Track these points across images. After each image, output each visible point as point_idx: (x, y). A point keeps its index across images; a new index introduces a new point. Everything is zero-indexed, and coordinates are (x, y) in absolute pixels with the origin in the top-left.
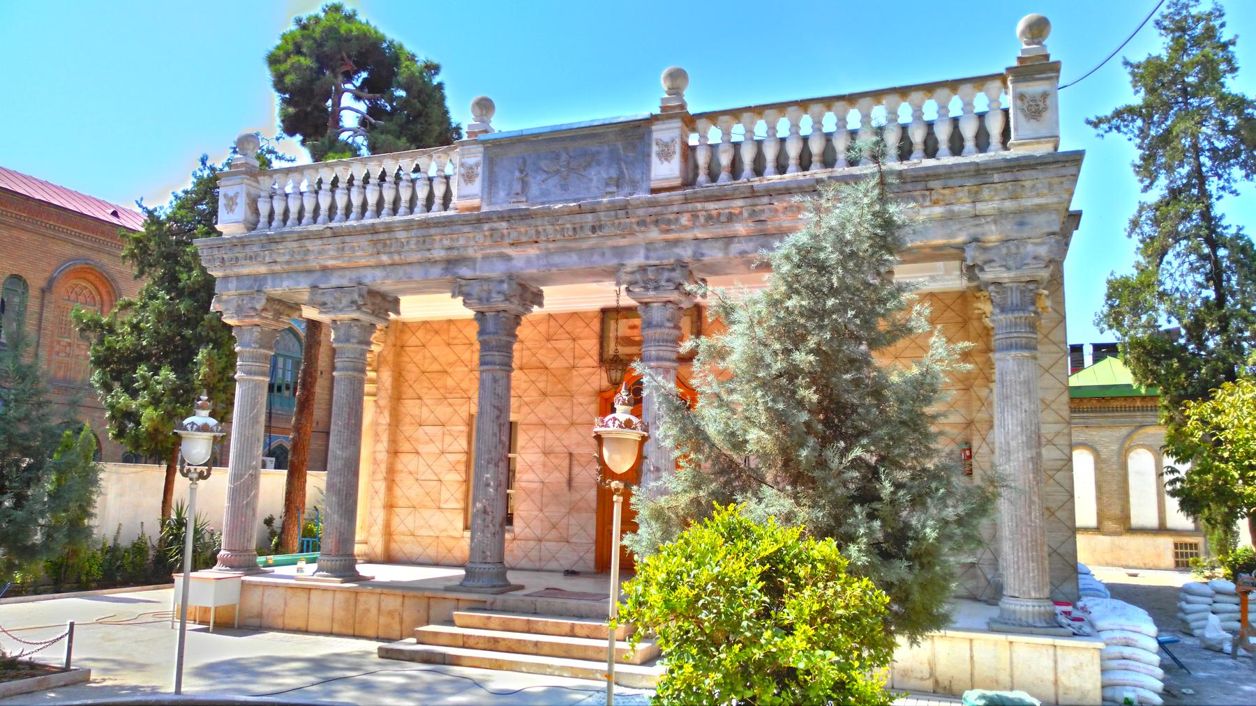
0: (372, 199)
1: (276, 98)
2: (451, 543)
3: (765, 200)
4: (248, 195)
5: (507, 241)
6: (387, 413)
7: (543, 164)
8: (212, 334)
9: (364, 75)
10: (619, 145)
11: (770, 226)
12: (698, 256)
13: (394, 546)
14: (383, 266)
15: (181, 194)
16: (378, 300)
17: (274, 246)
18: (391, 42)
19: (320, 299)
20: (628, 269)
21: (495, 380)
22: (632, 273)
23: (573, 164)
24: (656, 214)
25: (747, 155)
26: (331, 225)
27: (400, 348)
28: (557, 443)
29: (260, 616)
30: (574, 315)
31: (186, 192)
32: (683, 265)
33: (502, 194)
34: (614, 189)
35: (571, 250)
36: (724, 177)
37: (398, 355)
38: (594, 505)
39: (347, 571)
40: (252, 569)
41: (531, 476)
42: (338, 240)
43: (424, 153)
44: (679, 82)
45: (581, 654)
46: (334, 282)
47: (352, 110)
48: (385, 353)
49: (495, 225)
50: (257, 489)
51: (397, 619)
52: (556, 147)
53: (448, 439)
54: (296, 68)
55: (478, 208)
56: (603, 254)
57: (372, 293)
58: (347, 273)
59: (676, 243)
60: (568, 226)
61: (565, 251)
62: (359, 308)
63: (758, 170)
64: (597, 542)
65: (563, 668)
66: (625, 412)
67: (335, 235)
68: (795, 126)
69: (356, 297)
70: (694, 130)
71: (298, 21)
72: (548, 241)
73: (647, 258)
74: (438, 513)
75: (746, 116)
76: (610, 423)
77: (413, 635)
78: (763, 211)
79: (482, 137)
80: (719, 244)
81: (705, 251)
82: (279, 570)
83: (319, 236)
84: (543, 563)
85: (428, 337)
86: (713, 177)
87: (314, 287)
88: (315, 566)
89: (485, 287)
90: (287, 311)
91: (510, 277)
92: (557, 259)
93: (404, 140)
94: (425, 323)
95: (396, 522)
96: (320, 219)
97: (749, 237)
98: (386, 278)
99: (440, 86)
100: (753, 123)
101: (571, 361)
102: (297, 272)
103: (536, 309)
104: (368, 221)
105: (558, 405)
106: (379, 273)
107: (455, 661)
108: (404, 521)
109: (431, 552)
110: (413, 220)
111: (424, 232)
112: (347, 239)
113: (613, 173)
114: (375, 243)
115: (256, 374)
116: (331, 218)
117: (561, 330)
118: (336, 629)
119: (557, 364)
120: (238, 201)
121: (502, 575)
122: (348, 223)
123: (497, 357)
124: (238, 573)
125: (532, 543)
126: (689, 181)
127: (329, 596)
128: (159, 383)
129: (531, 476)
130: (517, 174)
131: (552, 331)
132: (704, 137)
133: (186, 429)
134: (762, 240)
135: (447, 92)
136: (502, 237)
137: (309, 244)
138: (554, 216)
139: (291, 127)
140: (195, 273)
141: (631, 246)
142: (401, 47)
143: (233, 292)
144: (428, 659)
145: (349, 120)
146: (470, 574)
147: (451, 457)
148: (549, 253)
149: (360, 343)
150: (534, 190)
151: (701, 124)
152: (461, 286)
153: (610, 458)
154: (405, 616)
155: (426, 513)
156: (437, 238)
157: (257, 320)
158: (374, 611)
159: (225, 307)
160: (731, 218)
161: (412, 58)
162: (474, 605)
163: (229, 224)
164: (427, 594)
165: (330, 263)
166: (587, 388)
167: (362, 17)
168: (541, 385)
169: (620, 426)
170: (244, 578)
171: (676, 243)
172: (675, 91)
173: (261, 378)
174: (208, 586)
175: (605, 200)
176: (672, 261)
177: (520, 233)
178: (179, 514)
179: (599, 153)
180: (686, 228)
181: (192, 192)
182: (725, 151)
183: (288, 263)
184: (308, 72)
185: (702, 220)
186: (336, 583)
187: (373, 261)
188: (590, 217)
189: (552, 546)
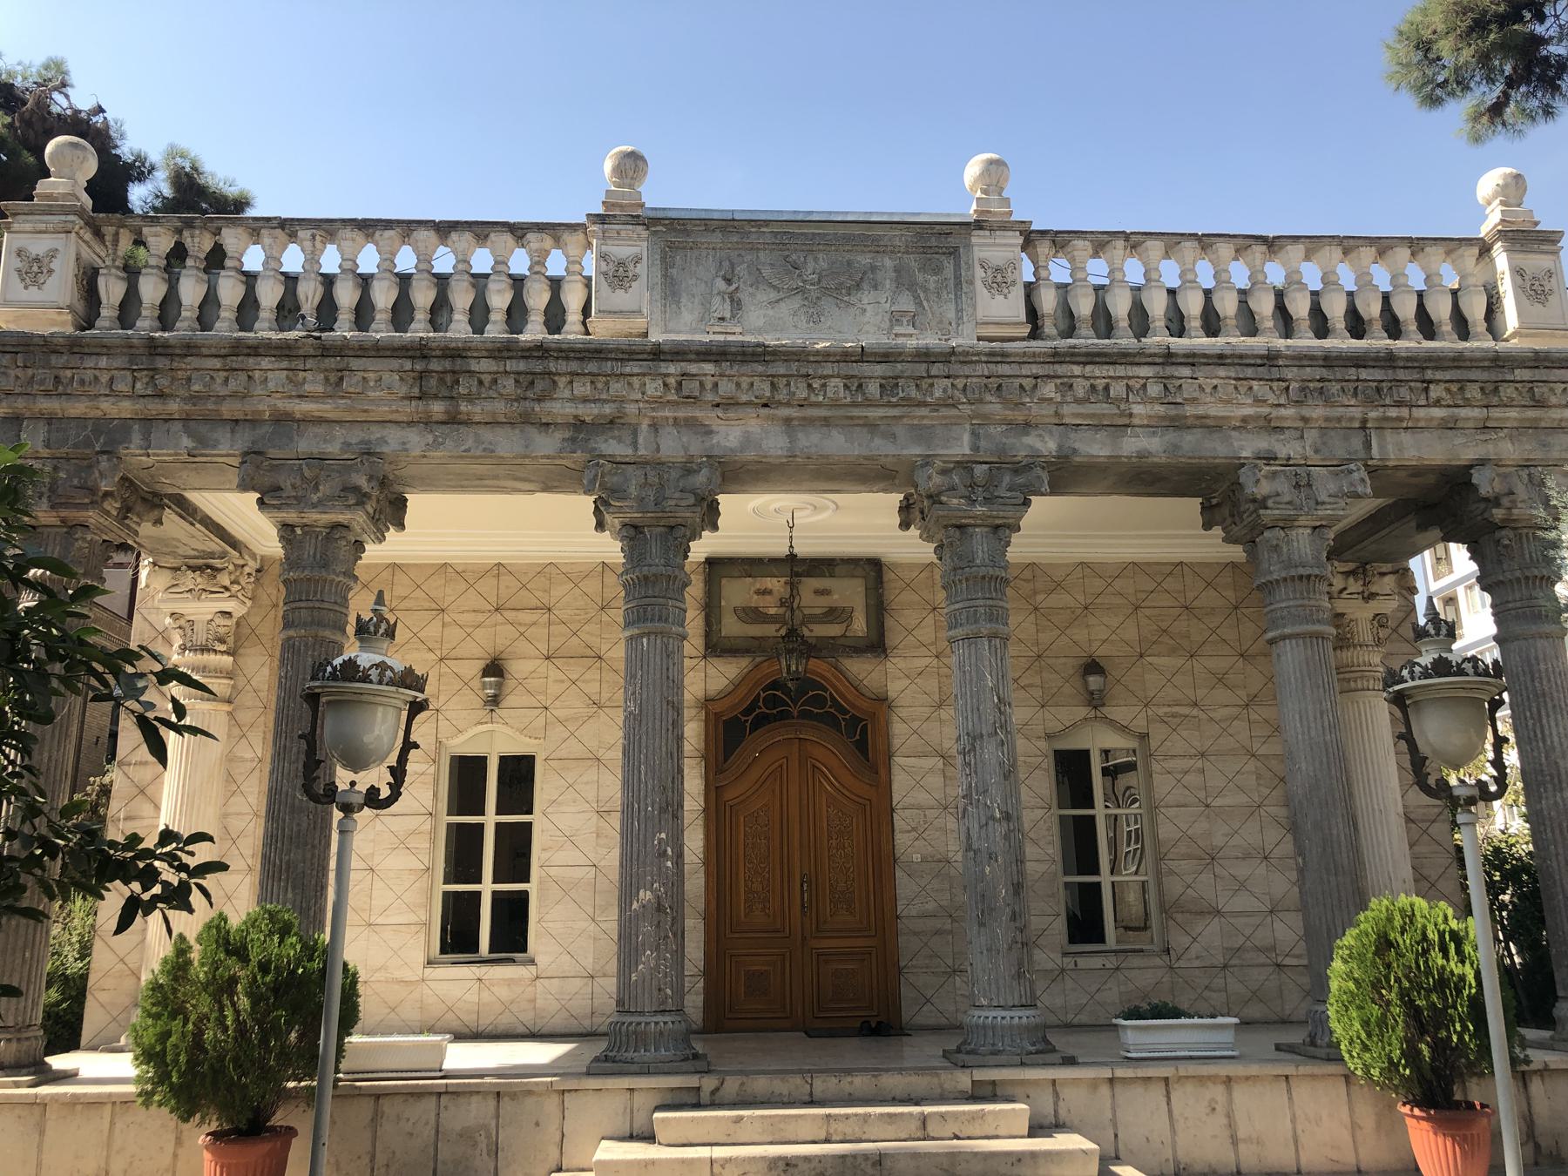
41: (572, 856)
46: (306, 444)
49: (693, 368)
58: (339, 432)
73: (975, 448)
98: (436, 444)
112: (355, 364)
129: (572, 856)
130: (720, 284)
133: (366, 679)
156: (562, 381)
162: (669, 1099)
168: (592, 688)
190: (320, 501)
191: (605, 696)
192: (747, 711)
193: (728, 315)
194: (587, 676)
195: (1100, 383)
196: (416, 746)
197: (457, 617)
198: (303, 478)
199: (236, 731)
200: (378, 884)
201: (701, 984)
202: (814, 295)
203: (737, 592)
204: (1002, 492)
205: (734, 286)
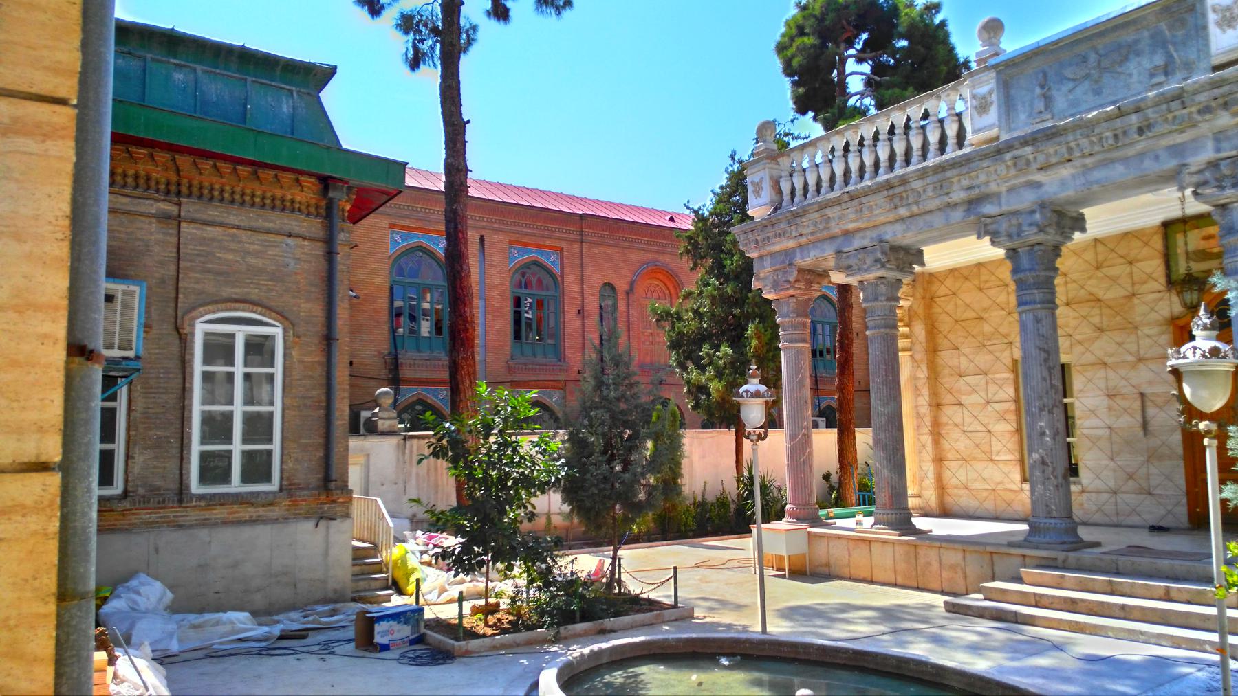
2: (1009, 496)
4: (771, 178)
5: (1034, 166)
6: (924, 367)
7: (1068, 73)
9: (864, 36)
10: (1163, 26)
13: (948, 500)
14: (902, 220)
16: (901, 255)
19: (845, 262)
20: (1193, 169)
21: (1038, 320)
22: (1200, 172)
24: (1223, 96)
27: (929, 301)
28: (1124, 383)
29: (828, 565)
30: (1126, 235)
31: (722, 188)
33: (1023, 117)
34: (1162, 78)
35: (1113, 161)
38: (1180, 450)
40: (816, 521)
42: (855, 202)
43: (932, 95)
46: (857, 243)
48: (915, 307)
49: (1017, 153)
51: (960, 574)
52: (1081, 49)
55: (997, 138)
56: (1157, 158)
57: (895, 249)
58: (868, 233)
60: (1108, 134)
62: (883, 266)
64: (1188, 493)
67: (852, 198)
69: (879, 255)
72: (1083, 156)
73: (1218, 150)
74: (991, 464)
76: (1189, 354)
77: (979, 591)
79: (993, 61)
82: (839, 523)
83: (837, 202)
84: (1121, 518)
85: (958, 285)
88: (871, 520)
89: (1014, 221)
91: (1042, 206)
92: (1097, 175)
93: (911, 89)
94: (952, 271)
95: (947, 475)
98: (908, 229)
99: (943, 24)
101: (1130, 289)
102: (822, 240)
103: (1077, 235)
105: (1119, 340)
106: (899, 227)
108: (956, 475)
109: (989, 505)
111: (940, 176)
112: (864, 200)
113: (1159, 60)
115: (797, 341)
116: (846, 183)
118: (900, 581)
119: (1112, 294)
121: (1073, 530)
123: (1037, 295)
125: (1105, 496)
127: (889, 548)
129: (1094, 422)
130: (1038, 91)
131: (1101, 258)
136: (1028, 163)
138: (1091, 125)
139: (802, 107)
141: (1194, 140)
145: (855, 84)
146: (1034, 529)
147: (997, 406)
148: (1086, 170)
149: (888, 300)
150: (1060, 102)
152: (986, 225)
153: (1193, 394)
154: (968, 570)
155: (979, 466)
156: (955, 180)
157: (791, 292)
158: (935, 565)
159: (764, 285)
162: (1044, 562)
163: (758, 209)
164: (989, 549)
165: (851, 226)
166: (1154, 316)
168: (1096, 320)
169: (1204, 355)
170: (810, 530)
174: (780, 536)
175: (1151, 94)
177: (1048, 156)
179: (1136, 42)
181: (727, 186)
183: (812, 233)
186: (894, 536)
187: (891, 217)
188: (1134, 118)
189: (1131, 499)
193: (1043, 109)
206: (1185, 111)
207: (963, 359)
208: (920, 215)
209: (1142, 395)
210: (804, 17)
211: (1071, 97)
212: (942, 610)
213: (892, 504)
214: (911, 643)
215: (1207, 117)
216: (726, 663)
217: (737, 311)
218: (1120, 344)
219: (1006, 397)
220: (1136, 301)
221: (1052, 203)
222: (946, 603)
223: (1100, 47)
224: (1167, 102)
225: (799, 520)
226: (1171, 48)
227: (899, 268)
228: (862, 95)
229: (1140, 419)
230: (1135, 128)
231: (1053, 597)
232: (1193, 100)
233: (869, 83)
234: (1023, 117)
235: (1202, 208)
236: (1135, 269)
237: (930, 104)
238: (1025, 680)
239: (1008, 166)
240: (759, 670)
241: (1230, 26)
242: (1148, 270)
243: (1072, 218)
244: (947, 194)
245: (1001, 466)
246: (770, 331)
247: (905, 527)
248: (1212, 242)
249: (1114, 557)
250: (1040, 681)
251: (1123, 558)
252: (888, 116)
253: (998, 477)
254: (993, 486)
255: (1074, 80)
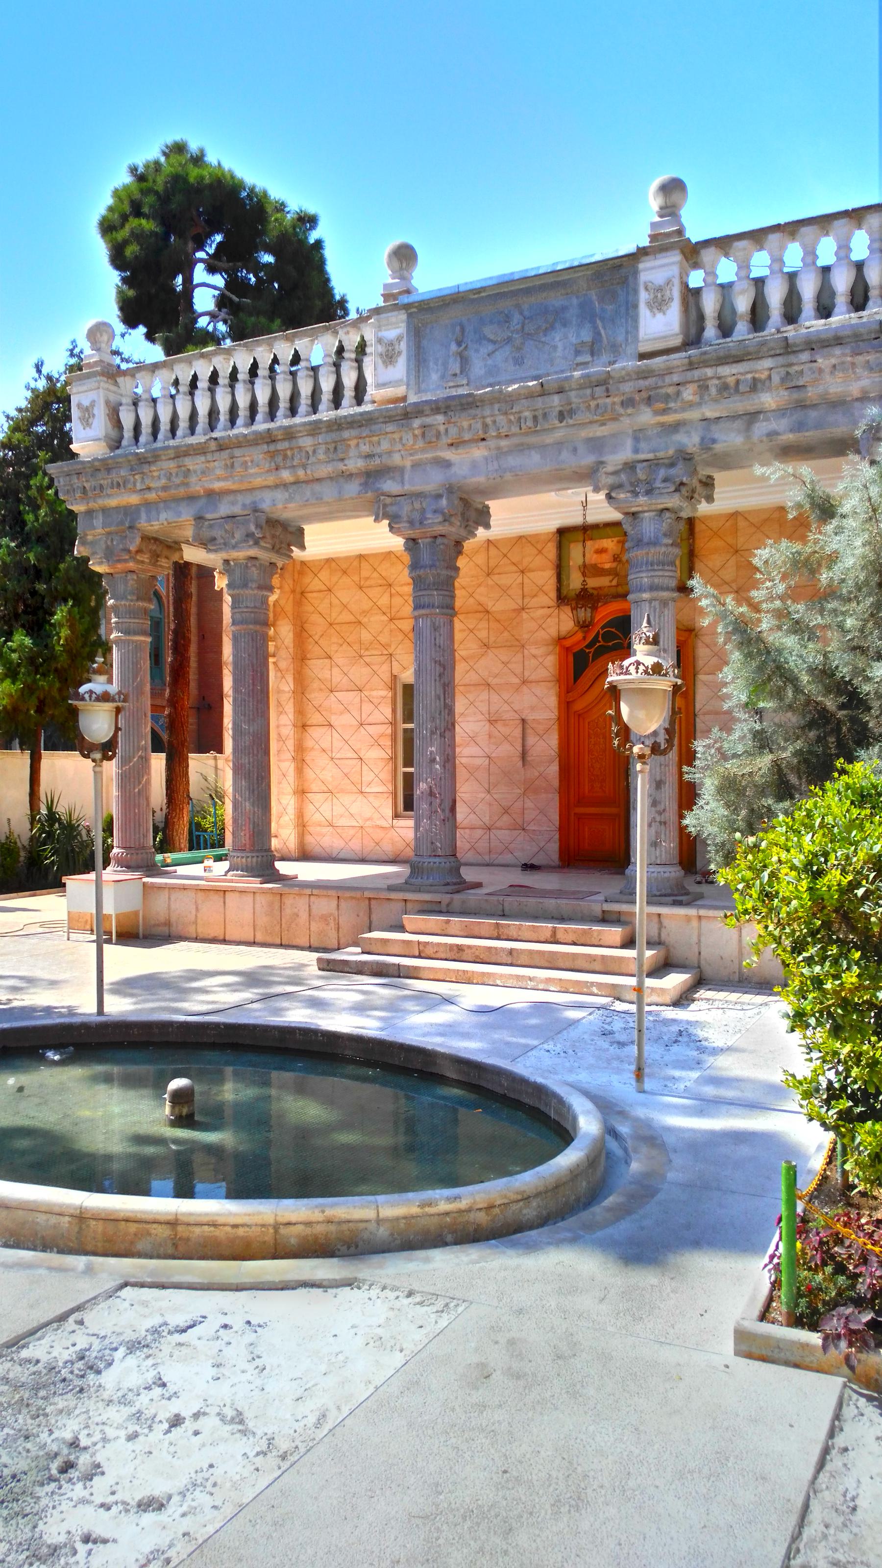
0: (263, 396)
1: (114, 277)
2: (378, 835)
3: (805, 356)
4: (107, 402)
5: (445, 440)
6: (290, 679)
7: (488, 331)
8: (69, 588)
9: (218, 238)
10: (593, 295)
11: (812, 393)
12: (707, 444)
13: (309, 839)
14: (285, 486)
15: (14, 413)
16: (279, 531)
17: (146, 468)
18: (252, 190)
19: (207, 533)
20: (610, 468)
21: (435, 628)
22: (616, 473)
23: (530, 328)
24: (648, 389)
25: (775, 296)
26: (215, 434)
27: (300, 595)
28: (506, 707)
29: (168, 923)
30: (520, 539)
31: (20, 410)
32: (686, 457)
33: (435, 377)
34: (587, 358)
35: (530, 447)
36: (742, 329)
37: (298, 604)
38: (556, 783)
39: (265, 869)
40: (151, 869)
42: (225, 454)
43: (327, 329)
44: (675, 197)
45: (568, 965)
46: (224, 509)
47: (206, 292)
48: (282, 602)
49: (428, 420)
50: (149, 774)
51: (332, 925)
52: (506, 305)
53: (367, 708)
54: (137, 236)
55: (404, 399)
56: (575, 450)
57: (273, 523)
58: (240, 498)
59: (676, 427)
60: (527, 414)
61: (522, 448)
62: (256, 543)
63: (791, 315)
64: (561, 829)
65: (548, 980)
66: (649, 654)
67: (221, 448)
68: (844, 248)
69: (252, 528)
70: (696, 266)
71: (133, 170)
72: (499, 437)
73: (636, 451)
74: (360, 797)
75: (773, 238)
76: (632, 669)
77: (355, 944)
78: (802, 372)
79: (405, 299)
80: (738, 424)
81: (716, 436)
82: (181, 870)
83: (200, 450)
84: (494, 856)
85: (335, 579)
86: (725, 330)
87: (199, 518)
88: (225, 865)
89: (417, 505)
90: (166, 552)
91: (450, 490)
92: (512, 461)
93: (278, 322)
94: (329, 561)
95: (310, 809)
96: (199, 428)
97: (781, 412)
98: (290, 499)
99: (319, 244)
100: (783, 248)
101: (520, 602)
102: (177, 500)
103: (481, 532)
104: (261, 425)
105: (505, 658)
106: (280, 496)
107: (413, 974)
108: (321, 809)
109: (355, 845)
110: (320, 421)
111: (334, 436)
112: (237, 452)
113: (586, 335)
114: (272, 455)
115: (136, 633)
116: (212, 427)
117: (505, 560)
118: (259, 938)
119: (501, 606)
120: (96, 411)
121: (455, 870)
122: (235, 431)
123: (436, 597)
124: (137, 875)
125: (479, 832)
126: (693, 337)
127: (249, 898)
128: (14, 651)
130: (454, 347)
131: (492, 563)
132: (711, 273)
133: (83, 699)
134: (797, 416)
135: (330, 253)
136: (438, 435)
137: (190, 463)
138: (510, 400)
139: (130, 319)
140: (42, 512)
141: (613, 436)
142: (265, 194)
143: (100, 531)
144: (379, 971)
145: (204, 300)
146: (416, 870)
147: (372, 729)
148: (500, 453)
149: (260, 588)
150: (478, 368)
151: (707, 255)
152: (385, 506)
153: (631, 715)
154: (343, 920)
155: (346, 799)
156: (353, 443)
157: (131, 565)
158: (304, 916)
159: (92, 549)
160: (755, 386)
161: (281, 207)
162: (426, 907)
163: (87, 441)
164: (367, 894)
165: (217, 485)
166: (541, 635)
167: (211, 158)
168: (483, 634)
169: (646, 672)
170: (146, 880)
171: (676, 427)
172: (670, 211)
173: (142, 638)
174: (106, 890)
175: (577, 374)
176: (671, 452)
177: (461, 429)
178: (50, 809)
179: (564, 309)
180: (691, 405)
181: (27, 410)
182: (743, 292)
183: (165, 488)
184: (153, 240)
185: (713, 391)
186: (254, 884)
187: (271, 480)
188: (556, 400)
189: (504, 835)
190: (237, 543)
191: (492, 639)
192: (589, 646)
193: (458, 372)
194: (480, 626)
195: (731, 381)
196: (120, 729)
197: (398, 589)
198: (226, 531)
199: (279, 674)
200: (365, 767)
201: (557, 836)
202: (518, 342)
203: (576, 554)
204: (658, 484)
205: (464, 346)
206: (608, 400)
207: (336, 670)
208: (307, 482)
209: (523, 720)
210: (142, 191)
211: (490, 362)
212: (314, 970)
213: (253, 845)
214: (288, 1009)
215: (629, 411)
216: (57, 1058)
217: (42, 587)
218: (505, 664)
219: (382, 718)
220: (525, 615)
221: (460, 488)
222: (319, 960)
223: (525, 307)
224: (592, 387)
225: (129, 867)
226: (599, 322)
227: (275, 549)
228: (213, 316)
229: (520, 749)
230: (555, 413)
231: (439, 944)
232: (618, 389)
233: (222, 302)
234: (435, 377)
235: (615, 515)
236: (526, 580)
237: (301, 344)
238: (438, 1040)
239: (415, 436)
240: (101, 1061)
241: (660, 310)
242: (540, 582)
243: (477, 510)
244: (342, 460)
245: (371, 799)
246: (87, 619)
247: (267, 873)
248: (605, 557)
249: (501, 898)
250: (438, 1040)
251: (510, 899)
252: (271, 346)
253: (368, 812)
254: (361, 823)
255: (494, 342)
